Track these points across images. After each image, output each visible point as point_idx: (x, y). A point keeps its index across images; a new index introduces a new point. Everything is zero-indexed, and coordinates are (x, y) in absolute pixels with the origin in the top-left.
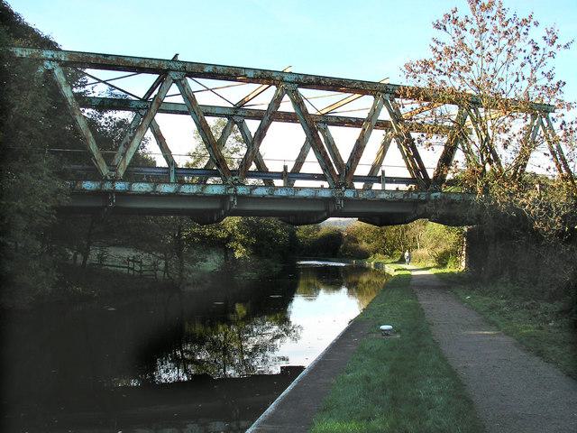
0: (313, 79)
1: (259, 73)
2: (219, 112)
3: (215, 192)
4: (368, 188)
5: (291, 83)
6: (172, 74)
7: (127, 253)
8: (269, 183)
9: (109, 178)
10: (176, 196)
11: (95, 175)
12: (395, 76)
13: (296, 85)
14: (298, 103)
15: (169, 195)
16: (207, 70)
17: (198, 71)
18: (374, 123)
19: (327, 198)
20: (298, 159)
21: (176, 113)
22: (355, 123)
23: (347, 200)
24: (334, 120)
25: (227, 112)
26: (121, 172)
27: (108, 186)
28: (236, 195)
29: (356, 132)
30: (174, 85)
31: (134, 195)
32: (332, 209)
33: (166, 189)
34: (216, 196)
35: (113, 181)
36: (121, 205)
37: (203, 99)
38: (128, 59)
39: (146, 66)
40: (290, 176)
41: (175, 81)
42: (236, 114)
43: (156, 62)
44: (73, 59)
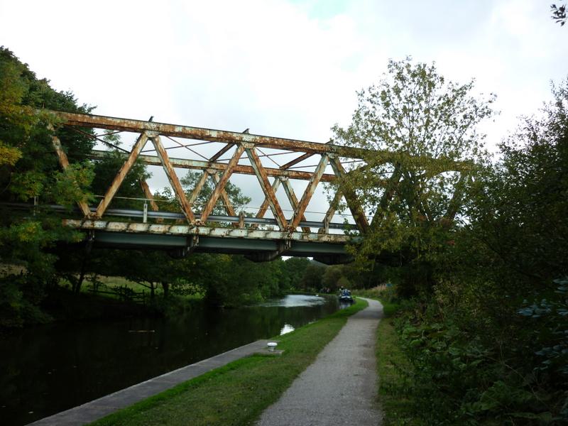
0: (268, 139)
1: (222, 133)
2: (156, 161)
3: (180, 232)
4: (322, 232)
5: (248, 142)
6: (147, 133)
7: (121, 282)
8: (307, 231)
9: (89, 217)
10: (146, 234)
11: (79, 214)
12: (323, 136)
13: (253, 144)
14: (255, 159)
15: (141, 233)
16: (177, 130)
17: (169, 132)
18: (319, 177)
19: (277, 239)
20: (328, 212)
21: (302, 179)
22: (305, 176)
23: (293, 241)
24: (294, 174)
25: (202, 165)
26: (100, 213)
27: (88, 224)
28: (198, 235)
29: (306, 183)
30: (150, 142)
31: (111, 232)
32: (282, 249)
33: (139, 228)
34: (181, 235)
35: (94, 219)
36: (290, 257)
37: (265, 163)
38: (110, 119)
39: (126, 125)
40: (325, 225)
41: (150, 139)
42: (284, 173)
43: (134, 123)
44: (130, 126)
